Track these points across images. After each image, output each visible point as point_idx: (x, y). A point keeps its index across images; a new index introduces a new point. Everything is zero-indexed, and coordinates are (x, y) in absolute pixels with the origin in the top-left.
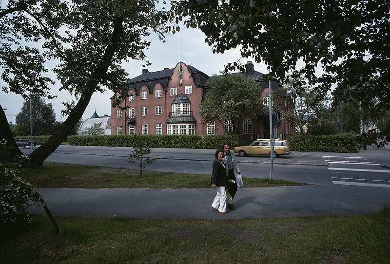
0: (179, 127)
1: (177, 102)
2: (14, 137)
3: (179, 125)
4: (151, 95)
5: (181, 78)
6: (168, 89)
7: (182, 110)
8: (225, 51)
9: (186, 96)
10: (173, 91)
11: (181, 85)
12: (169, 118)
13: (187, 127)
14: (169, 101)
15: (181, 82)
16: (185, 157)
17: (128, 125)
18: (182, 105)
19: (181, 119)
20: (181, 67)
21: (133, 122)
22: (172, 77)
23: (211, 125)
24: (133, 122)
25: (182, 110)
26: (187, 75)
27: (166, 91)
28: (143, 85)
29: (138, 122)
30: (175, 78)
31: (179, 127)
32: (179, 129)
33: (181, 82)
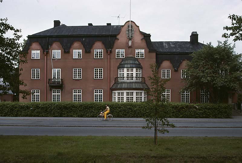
0: (125, 94)
1: (129, 66)
2: (143, 100)
3: (135, 92)
4: (88, 54)
5: (130, 39)
6: (113, 50)
7: (134, 75)
8: (53, 27)
9: (137, 59)
10: (121, 52)
11: (130, 47)
12: (116, 85)
13: (135, 94)
14: (114, 64)
15: (130, 43)
16: (9, 124)
17: (51, 90)
18: (134, 70)
19: (137, 86)
20: (132, 27)
21: (59, 86)
22: (118, 37)
23: (35, 94)
24: (59, 86)
25: (134, 75)
26: (138, 38)
27: (48, 53)
28: (77, 41)
29: (67, 86)
30: (122, 38)
31: (125, 94)
32: (125, 96)
33: (130, 43)
